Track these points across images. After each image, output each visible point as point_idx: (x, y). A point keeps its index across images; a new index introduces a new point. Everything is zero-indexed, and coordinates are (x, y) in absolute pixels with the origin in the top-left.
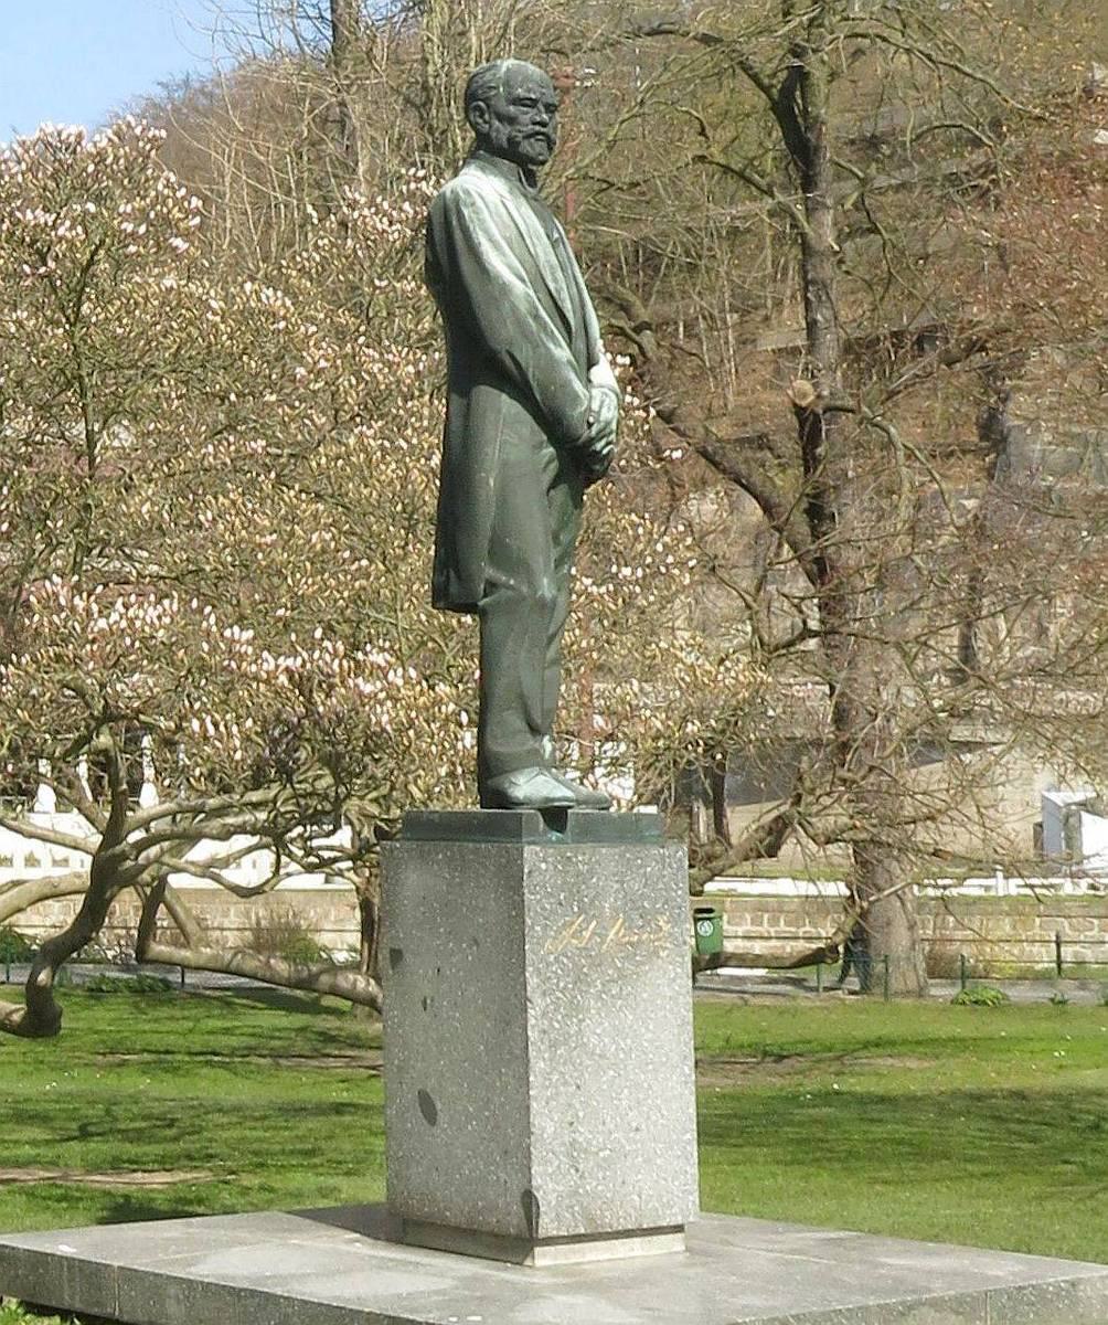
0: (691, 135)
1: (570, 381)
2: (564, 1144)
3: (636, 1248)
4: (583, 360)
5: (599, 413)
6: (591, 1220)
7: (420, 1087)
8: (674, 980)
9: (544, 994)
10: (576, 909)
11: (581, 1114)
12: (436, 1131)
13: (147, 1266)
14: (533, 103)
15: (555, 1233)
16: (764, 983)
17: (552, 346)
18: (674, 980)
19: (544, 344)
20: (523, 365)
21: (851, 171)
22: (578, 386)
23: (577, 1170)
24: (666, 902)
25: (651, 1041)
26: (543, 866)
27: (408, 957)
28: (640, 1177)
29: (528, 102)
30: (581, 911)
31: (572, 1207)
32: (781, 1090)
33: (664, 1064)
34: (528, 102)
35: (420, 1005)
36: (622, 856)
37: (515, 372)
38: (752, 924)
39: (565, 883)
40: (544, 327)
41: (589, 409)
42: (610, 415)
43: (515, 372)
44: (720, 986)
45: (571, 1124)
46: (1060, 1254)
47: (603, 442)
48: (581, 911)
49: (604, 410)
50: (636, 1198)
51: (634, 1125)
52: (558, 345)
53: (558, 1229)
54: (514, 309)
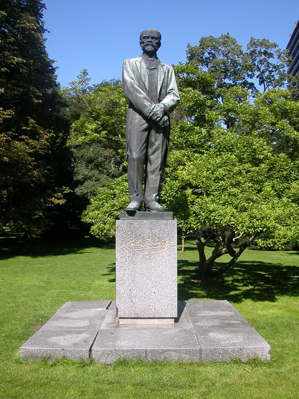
3: (156, 321)
10: (134, 236)
11: (134, 288)
13: (273, 253)
14: (148, 37)
15: (123, 316)
16: (290, 44)
17: (138, 94)
20: (130, 100)
21: (228, 320)
23: (132, 302)
26: (123, 225)
28: (155, 304)
29: (146, 37)
30: (135, 237)
32: (65, 115)
34: (146, 37)
37: (258, 263)
43: (258, 263)
44: (162, 210)
48: (135, 237)
50: (154, 310)
54: (127, 86)
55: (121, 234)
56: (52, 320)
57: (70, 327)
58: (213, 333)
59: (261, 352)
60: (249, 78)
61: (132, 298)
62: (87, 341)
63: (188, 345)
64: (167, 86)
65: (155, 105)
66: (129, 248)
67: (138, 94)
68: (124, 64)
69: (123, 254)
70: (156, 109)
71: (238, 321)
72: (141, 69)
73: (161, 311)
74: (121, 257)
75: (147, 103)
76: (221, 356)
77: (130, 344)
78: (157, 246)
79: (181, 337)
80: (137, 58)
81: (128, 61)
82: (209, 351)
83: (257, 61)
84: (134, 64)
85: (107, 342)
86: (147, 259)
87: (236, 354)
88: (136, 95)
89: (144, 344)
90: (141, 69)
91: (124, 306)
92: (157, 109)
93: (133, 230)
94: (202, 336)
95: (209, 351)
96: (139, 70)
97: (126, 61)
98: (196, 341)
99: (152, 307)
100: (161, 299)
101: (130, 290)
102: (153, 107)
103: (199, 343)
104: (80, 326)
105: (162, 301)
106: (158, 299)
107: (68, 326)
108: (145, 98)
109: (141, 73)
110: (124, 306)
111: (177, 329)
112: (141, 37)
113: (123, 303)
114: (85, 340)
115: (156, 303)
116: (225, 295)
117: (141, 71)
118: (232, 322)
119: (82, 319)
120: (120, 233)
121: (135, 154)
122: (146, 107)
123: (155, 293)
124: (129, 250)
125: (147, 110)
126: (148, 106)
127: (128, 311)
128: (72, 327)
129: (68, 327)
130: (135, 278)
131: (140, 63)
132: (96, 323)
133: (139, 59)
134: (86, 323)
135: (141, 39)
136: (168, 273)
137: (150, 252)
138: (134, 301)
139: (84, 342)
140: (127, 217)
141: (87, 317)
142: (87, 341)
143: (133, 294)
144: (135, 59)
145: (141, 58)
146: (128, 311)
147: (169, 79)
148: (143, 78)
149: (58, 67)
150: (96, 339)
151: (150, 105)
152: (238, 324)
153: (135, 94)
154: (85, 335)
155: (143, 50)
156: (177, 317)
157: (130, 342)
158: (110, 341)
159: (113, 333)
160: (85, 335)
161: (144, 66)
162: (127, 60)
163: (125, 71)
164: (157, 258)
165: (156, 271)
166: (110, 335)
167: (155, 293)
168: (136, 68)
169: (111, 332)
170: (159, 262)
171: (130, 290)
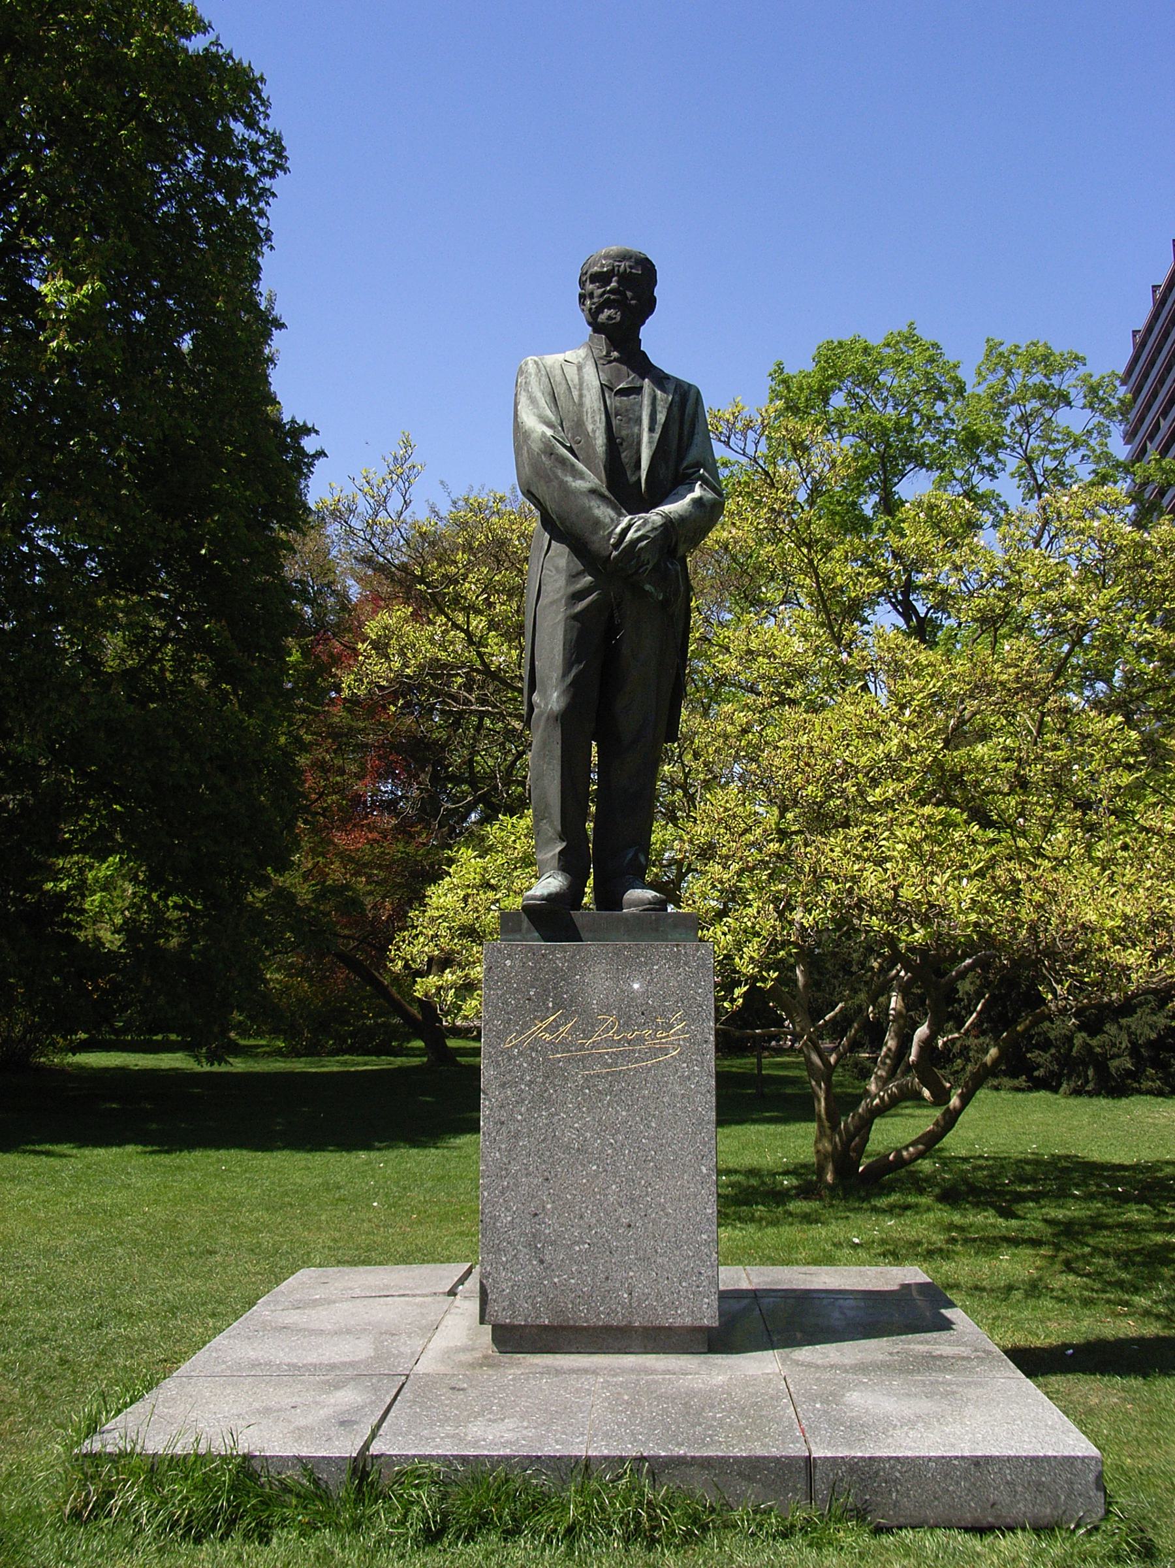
17: (569, 479)
26: (508, 963)
28: (631, 1274)
55: (503, 994)
56: (230, 1337)
57: (295, 1366)
58: (861, 1391)
59: (1066, 1482)
60: (988, 478)
61: (543, 1246)
62: (355, 1422)
63: (758, 1439)
64: (679, 447)
65: (629, 517)
66: (532, 1049)
67: (569, 479)
68: (521, 372)
69: (510, 1071)
70: (636, 531)
71: (963, 1349)
72: (581, 390)
73: (657, 1300)
74: (503, 1085)
75: (603, 512)
76: (897, 1491)
77: (524, 1432)
78: (640, 1040)
79: (733, 1408)
80: (568, 353)
81: (536, 362)
82: (844, 1468)
83: (1011, 418)
84: (558, 372)
85: (432, 1424)
86: (599, 1092)
87: (958, 1483)
88: (563, 486)
89: (583, 1434)
90: (581, 390)
91: (510, 1279)
92: (639, 533)
93: (548, 982)
94: (818, 1406)
95: (844, 1468)
96: (575, 394)
97: (526, 364)
98: (791, 1425)
99: (618, 1285)
100: (656, 1251)
101: (536, 1215)
102: (623, 525)
103: (803, 1431)
104: (336, 1359)
105: (659, 1260)
106: (641, 1253)
107: (287, 1360)
108: (593, 492)
109: (581, 404)
110: (510, 1279)
111: (718, 1374)
112: (583, 274)
113: (508, 1266)
114: (347, 1417)
115: (635, 1269)
116: (51, 547)
117: (581, 396)
118: (939, 1352)
119: (349, 1332)
120: (500, 992)
121: (558, 697)
122: (597, 523)
123: (629, 1226)
124: (533, 1059)
125: (604, 537)
126: (608, 520)
127: (526, 1298)
128: (304, 1365)
129: (288, 1365)
130: (553, 1164)
131: (580, 368)
132: (402, 1350)
133: (577, 354)
134: (360, 1349)
135: (582, 284)
136: (682, 1149)
137: (610, 1066)
138: (548, 1258)
139: (342, 1423)
140: (524, 931)
141: (370, 1324)
142: (355, 1422)
143: (547, 1231)
144: (560, 357)
145: (582, 352)
146: (526, 1298)
147: (686, 427)
148: (590, 420)
149: (317, 432)
150: (392, 1414)
151: (612, 520)
152: (963, 1358)
153: (557, 477)
154: (348, 1397)
155: (590, 324)
156: (717, 1324)
157: (525, 1424)
158: (448, 1419)
159: (463, 1389)
160: (348, 1397)
161: (592, 378)
162: (530, 359)
163: (523, 399)
164: (641, 1088)
165: (635, 1141)
166: (448, 1399)
167: (629, 1226)
168: (564, 386)
169: (453, 1385)
170: (647, 1105)
171: (536, 1215)
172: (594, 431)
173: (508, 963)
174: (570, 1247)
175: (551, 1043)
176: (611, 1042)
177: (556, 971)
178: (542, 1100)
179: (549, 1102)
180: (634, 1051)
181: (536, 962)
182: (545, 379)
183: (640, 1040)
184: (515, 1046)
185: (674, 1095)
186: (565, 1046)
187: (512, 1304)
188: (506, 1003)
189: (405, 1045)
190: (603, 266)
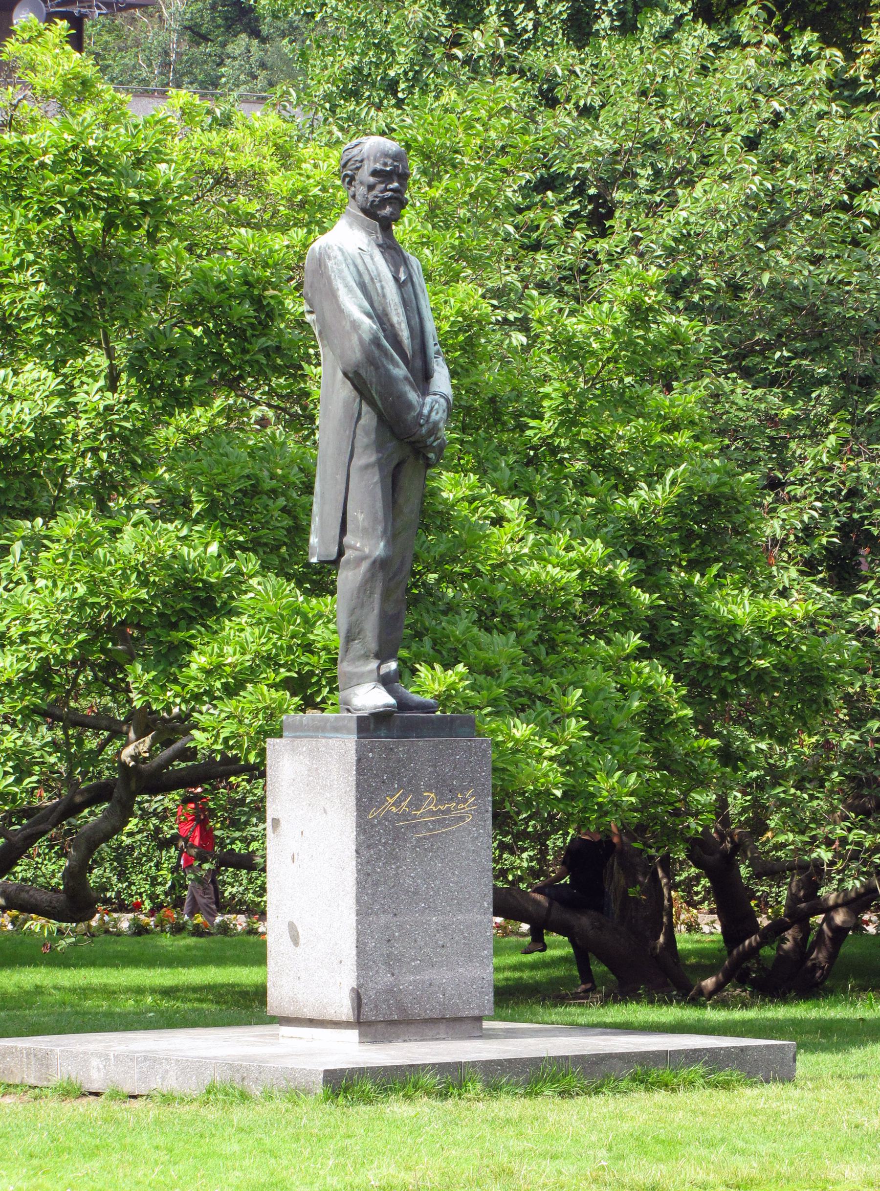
0: (592, 98)
1: (406, 393)
2: (382, 955)
4: (420, 375)
5: (429, 416)
6: (402, 1009)
7: (289, 919)
8: (477, 838)
9: (369, 847)
12: (299, 950)
17: (391, 367)
18: (477, 838)
19: (384, 366)
22: (413, 396)
24: (472, 781)
25: (457, 883)
26: (371, 755)
27: (283, 823)
30: (400, 787)
31: (388, 1000)
33: (465, 899)
35: (290, 859)
36: (436, 747)
38: (265, 822)
39: (388, 767)
40: (385, 353)
41: (420, 414)
42: (437, 417)
45: (389, 941)
46: (359, 933)
47: (432, 439)
49: (433, 414)
51: (441, 943)
52: (396, 365)
53: (376, 1016)
88: (387, 371)
109: (384, 296)
137: (431, 830)
172: (399, 323)
173: (371, 755)
174: (409, 963)
175: (396, 814)
176: (433, 813)
177: (399, 761)
178: (393, 857)
179: (396, 858)
180: (445, 819)
181: (388, 754)
182: (352, 267)
183: (449, 811)
184: (375, 817)
185: (468, 851)
186: (404, 816)
187: (376, 1006)
188: (370, 786)
189: (670, 791)
190: (385, 164)
